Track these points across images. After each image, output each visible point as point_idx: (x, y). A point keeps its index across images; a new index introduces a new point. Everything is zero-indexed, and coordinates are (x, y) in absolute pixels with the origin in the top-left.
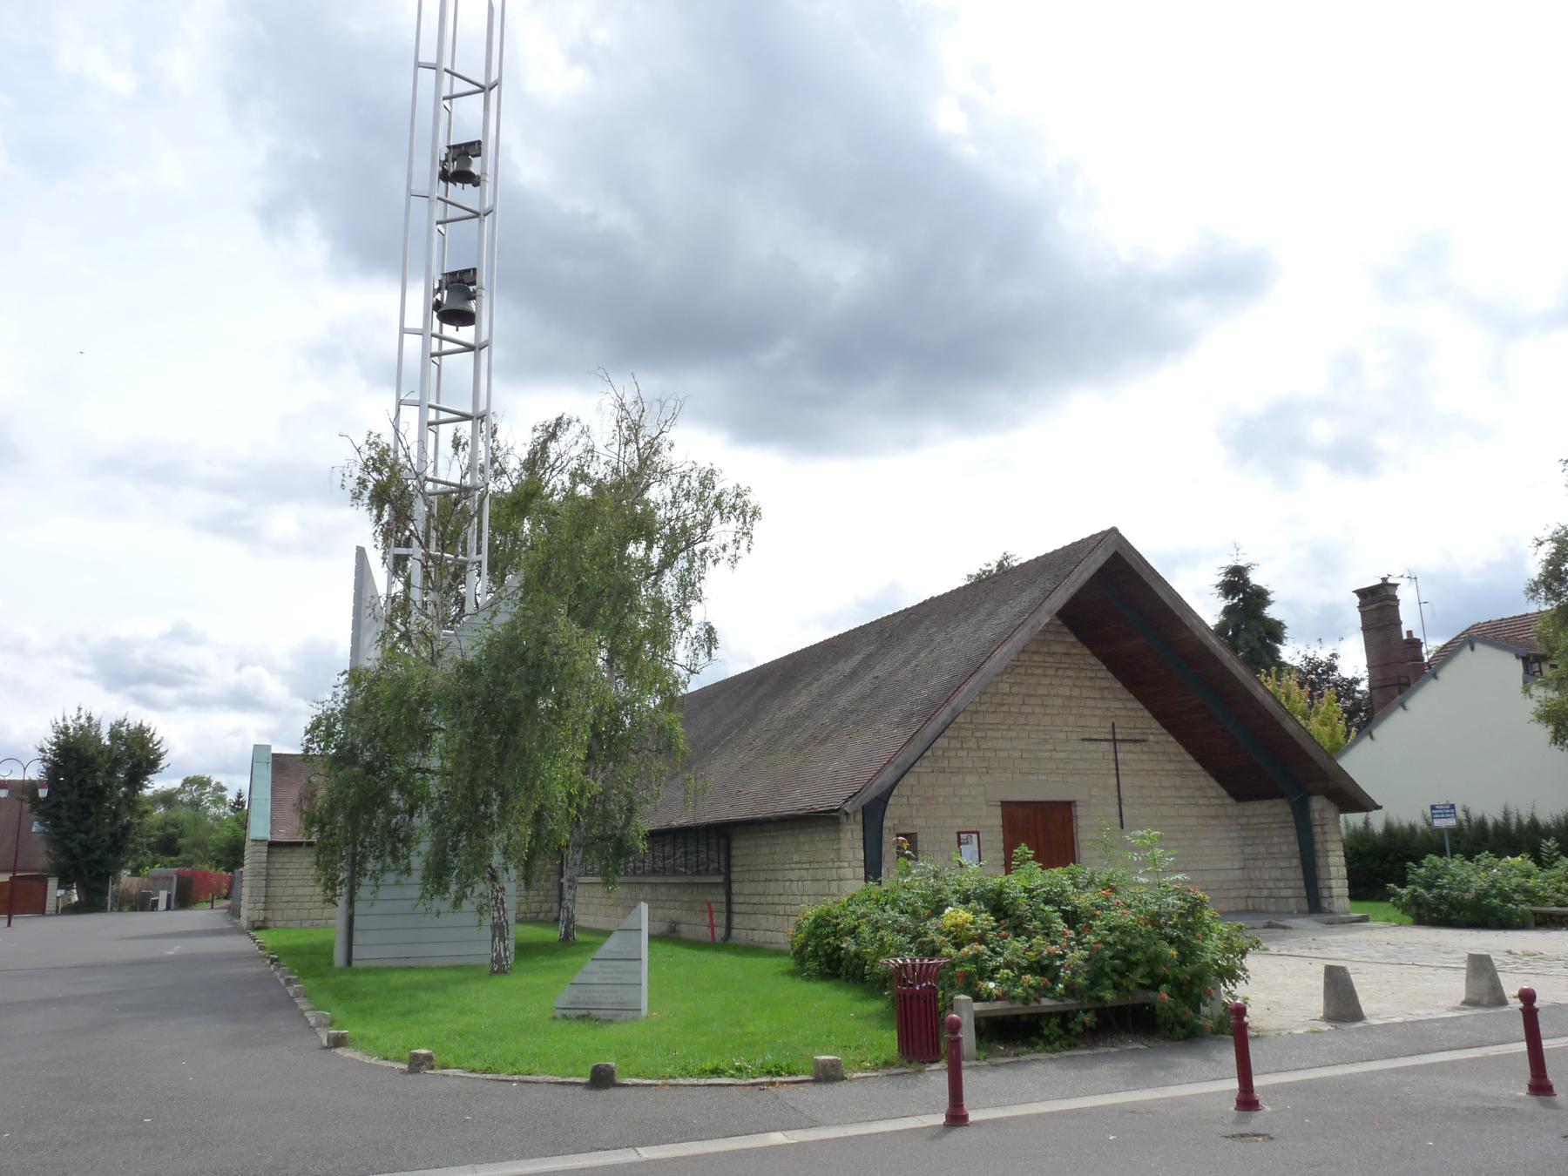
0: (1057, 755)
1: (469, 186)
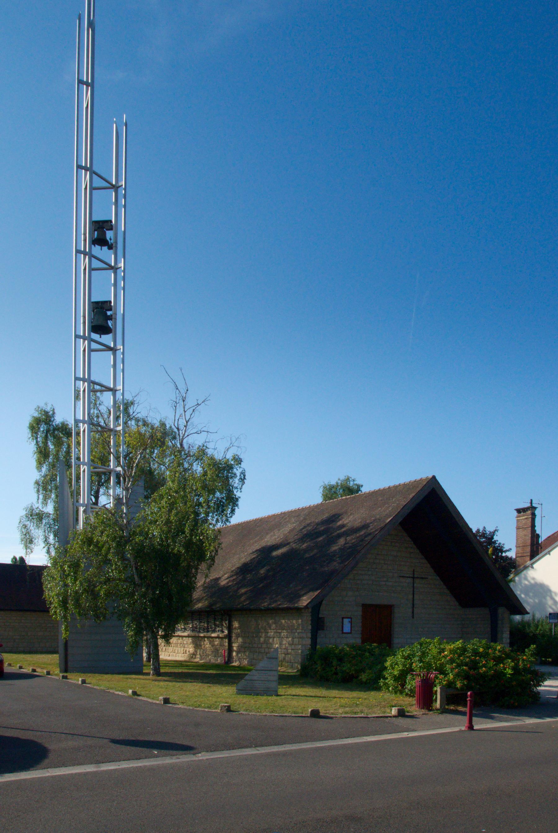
1: (105, 248)
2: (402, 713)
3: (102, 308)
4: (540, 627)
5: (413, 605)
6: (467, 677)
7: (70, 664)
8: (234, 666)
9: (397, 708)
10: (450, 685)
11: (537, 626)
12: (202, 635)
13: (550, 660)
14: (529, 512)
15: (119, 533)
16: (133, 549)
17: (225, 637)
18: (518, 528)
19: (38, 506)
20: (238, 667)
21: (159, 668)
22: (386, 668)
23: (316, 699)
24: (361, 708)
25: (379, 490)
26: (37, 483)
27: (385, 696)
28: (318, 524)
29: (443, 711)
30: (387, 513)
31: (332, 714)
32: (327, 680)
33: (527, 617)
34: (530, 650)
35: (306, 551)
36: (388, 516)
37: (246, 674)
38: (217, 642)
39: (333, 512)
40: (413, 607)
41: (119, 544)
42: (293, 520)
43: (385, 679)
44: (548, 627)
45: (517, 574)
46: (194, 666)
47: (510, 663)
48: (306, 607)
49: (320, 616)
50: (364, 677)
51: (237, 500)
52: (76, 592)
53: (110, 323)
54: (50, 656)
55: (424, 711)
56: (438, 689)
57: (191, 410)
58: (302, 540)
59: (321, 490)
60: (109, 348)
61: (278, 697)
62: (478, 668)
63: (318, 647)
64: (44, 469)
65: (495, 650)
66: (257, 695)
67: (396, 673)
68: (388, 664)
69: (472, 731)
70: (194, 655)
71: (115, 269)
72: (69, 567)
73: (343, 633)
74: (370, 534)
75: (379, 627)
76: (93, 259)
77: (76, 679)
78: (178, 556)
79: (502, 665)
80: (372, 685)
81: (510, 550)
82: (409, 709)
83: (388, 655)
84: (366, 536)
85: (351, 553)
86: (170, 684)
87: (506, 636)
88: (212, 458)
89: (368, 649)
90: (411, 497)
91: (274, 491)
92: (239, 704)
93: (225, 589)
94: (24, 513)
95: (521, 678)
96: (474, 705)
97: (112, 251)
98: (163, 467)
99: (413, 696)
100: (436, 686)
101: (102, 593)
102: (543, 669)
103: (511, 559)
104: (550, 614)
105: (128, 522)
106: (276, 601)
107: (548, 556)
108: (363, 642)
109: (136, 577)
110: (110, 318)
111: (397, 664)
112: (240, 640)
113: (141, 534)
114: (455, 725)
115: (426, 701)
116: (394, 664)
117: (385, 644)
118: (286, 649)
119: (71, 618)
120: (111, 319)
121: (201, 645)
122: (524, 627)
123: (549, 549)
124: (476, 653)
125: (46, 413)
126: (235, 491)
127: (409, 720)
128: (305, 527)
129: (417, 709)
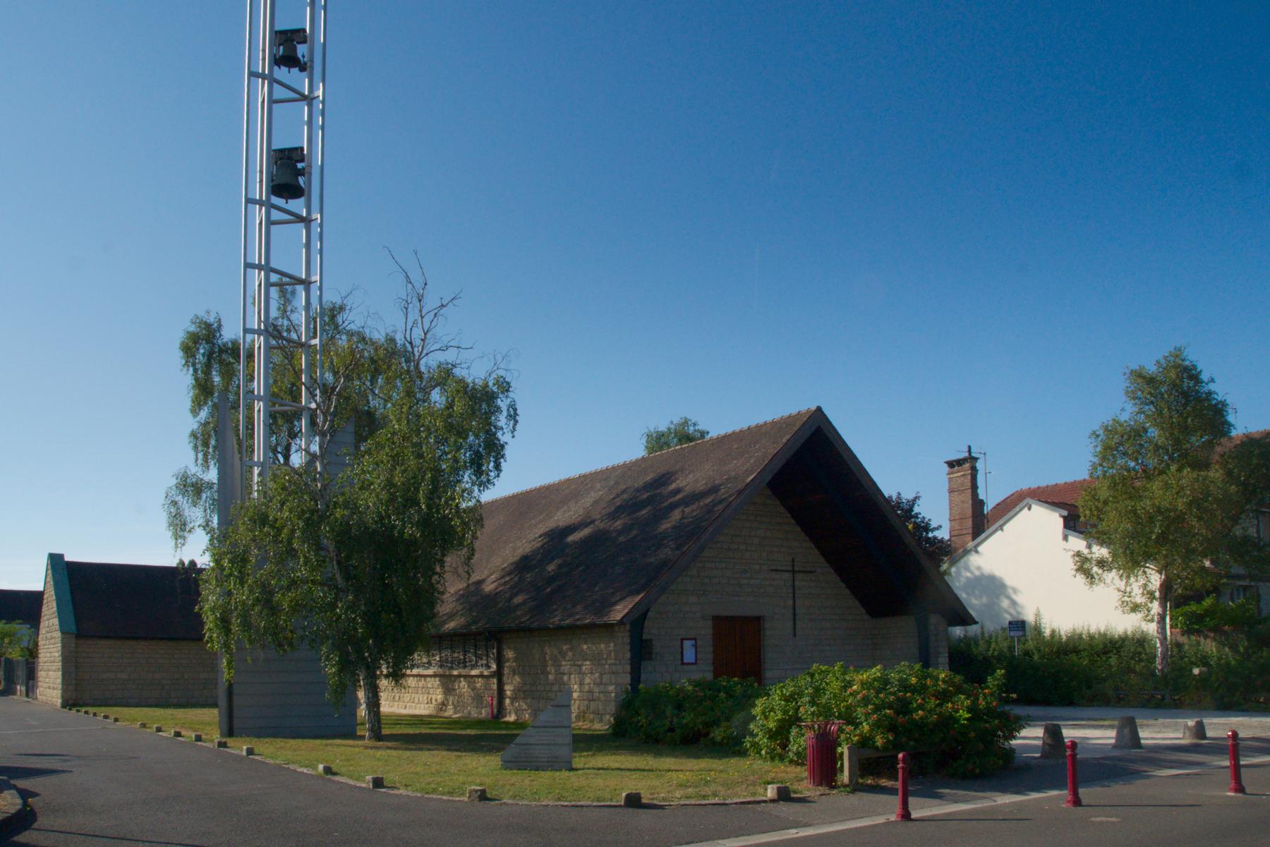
0: (753, 582)
1: (295, 70)
2: (784, 795)
3: (289, 158)
4: (993, 645)
5: (794, 615)
6: (892, 728)
7: (236, 722)
8: (507, 723)
9: (775, 786)
10: (865, 742)
11: (989, 643)
12: (455, 673)
13: (1015, 696)
14: (967, 465)
15: (312, 504)
16: (332, 530)
17: (492, 675)
18: (951, 491)
19: (195, 470)
20: (513, 723)
21: (380, 728)
22: (754, 717)
23: (637, 775)
24: (713, 787)
25: (734, 433)
26: (194, 435)
27: (755, 766)
28: (638, 490)
29: (855, 788)
30: (748, 468)
31: (664, 799)
32: (657, 741)
33: (973, 630)
34: (995, 679)
35: (620, 532)
36: (748, 472)
37: (516, 736)
38: (479, 683)
39: (662, 470)
40: (794, 620)
41: (308, 522)
42: (598, 485)
43: (753, 735)
44: (1005, 644)
45: (953, 562)
46: (443, 723)
47: (963, 701)
48: (621, 622)
49: (645, 637)
50: (717, 734)
51: (503, 447)
52: (244, 603)
53: (301, 180)
54: (206, 711)
55: (822, 789)
56: (844, 750)
57: (432, 314)
58: (613, 516)
59: (644, 440)
60: (300, 219)
61: (572, 773)
62: (911, 712)
63: (641, 686)
64: (204, 414)
65: (937, 679)
66: (537, 769)
67: (772, 725)
68: (757, 710)
69: (910, 824)
70: (443, 705)
71: (309, 100)
72: (230, 561)
73: (683, 664)
74: (721, 501)
75: (741, 652)
76: (275, 85)
77: (240, 747)
78: (412, 543)
79: (950, 705)
80: (733, 747)
81: (940, 527)
82: (795, 787)
83: (758, 696)
84: (715, 506)
85: (690, 533)
86: (394, 753)
87: (944, 659)
88: (461, 381)
89: (725, 687)
90: (784, 440)
91: (566, 439)
92: (504, 786)
93: (493, 597)
94: (174, 481)
95: (982, 725)
96: (910, 775)
97: (304, 74)
98: (383, 400)
99: (802, 764)
100: (840, 745)
101: (285, 605)
102: (1018, 711)
103: (942, 541)
104: (1010, 623)
105: (324, 487)
106: (571, 615)
107: (999, 532)
108: (716, 676)
109: (338, 577)
110: (301, 173)
111: (772, 710)
112: (517, 679)
113: (346, 505)
114: (878, 812)
115: (825, 771)
116: (765, 712)
117: (752, 679)
118: (590, 691)
119: (238, 648)
120: (303, 175)
121: (454, 690)
122: (968, 645)
123: (1001, 522)
124: (905, 686)
125: (208, 326)
126: (499, 434)
127: (797, 806)
128: (618, 496)
129: (811, 786)
